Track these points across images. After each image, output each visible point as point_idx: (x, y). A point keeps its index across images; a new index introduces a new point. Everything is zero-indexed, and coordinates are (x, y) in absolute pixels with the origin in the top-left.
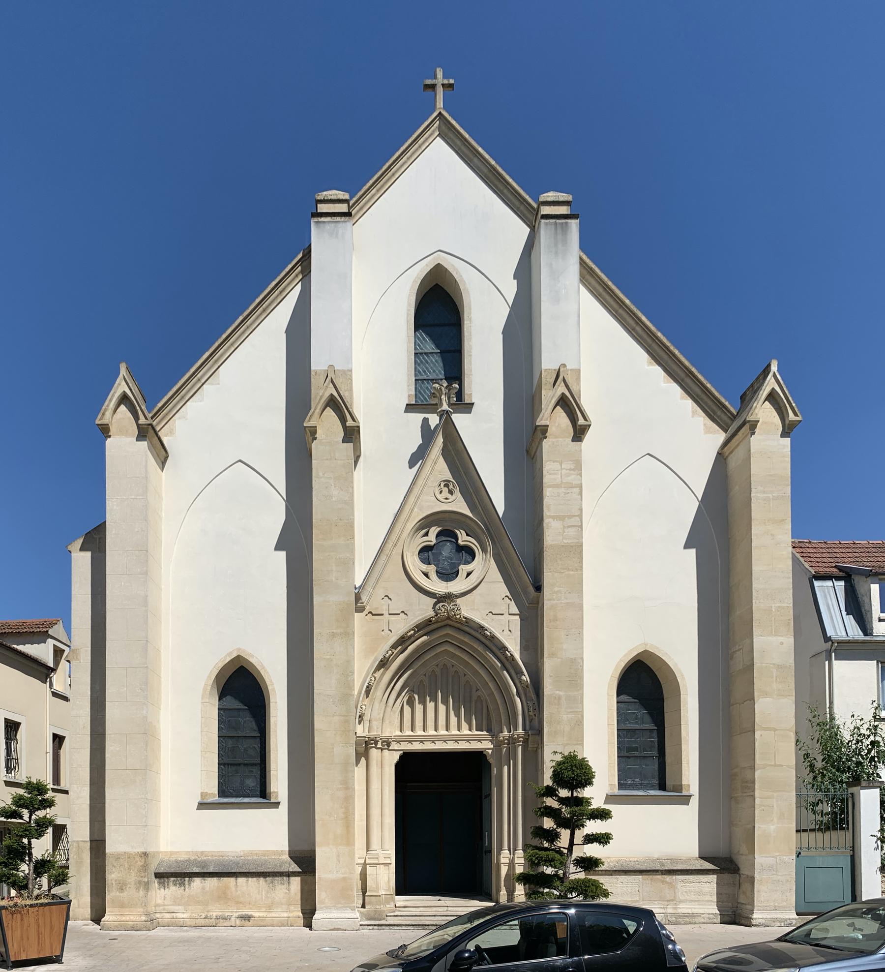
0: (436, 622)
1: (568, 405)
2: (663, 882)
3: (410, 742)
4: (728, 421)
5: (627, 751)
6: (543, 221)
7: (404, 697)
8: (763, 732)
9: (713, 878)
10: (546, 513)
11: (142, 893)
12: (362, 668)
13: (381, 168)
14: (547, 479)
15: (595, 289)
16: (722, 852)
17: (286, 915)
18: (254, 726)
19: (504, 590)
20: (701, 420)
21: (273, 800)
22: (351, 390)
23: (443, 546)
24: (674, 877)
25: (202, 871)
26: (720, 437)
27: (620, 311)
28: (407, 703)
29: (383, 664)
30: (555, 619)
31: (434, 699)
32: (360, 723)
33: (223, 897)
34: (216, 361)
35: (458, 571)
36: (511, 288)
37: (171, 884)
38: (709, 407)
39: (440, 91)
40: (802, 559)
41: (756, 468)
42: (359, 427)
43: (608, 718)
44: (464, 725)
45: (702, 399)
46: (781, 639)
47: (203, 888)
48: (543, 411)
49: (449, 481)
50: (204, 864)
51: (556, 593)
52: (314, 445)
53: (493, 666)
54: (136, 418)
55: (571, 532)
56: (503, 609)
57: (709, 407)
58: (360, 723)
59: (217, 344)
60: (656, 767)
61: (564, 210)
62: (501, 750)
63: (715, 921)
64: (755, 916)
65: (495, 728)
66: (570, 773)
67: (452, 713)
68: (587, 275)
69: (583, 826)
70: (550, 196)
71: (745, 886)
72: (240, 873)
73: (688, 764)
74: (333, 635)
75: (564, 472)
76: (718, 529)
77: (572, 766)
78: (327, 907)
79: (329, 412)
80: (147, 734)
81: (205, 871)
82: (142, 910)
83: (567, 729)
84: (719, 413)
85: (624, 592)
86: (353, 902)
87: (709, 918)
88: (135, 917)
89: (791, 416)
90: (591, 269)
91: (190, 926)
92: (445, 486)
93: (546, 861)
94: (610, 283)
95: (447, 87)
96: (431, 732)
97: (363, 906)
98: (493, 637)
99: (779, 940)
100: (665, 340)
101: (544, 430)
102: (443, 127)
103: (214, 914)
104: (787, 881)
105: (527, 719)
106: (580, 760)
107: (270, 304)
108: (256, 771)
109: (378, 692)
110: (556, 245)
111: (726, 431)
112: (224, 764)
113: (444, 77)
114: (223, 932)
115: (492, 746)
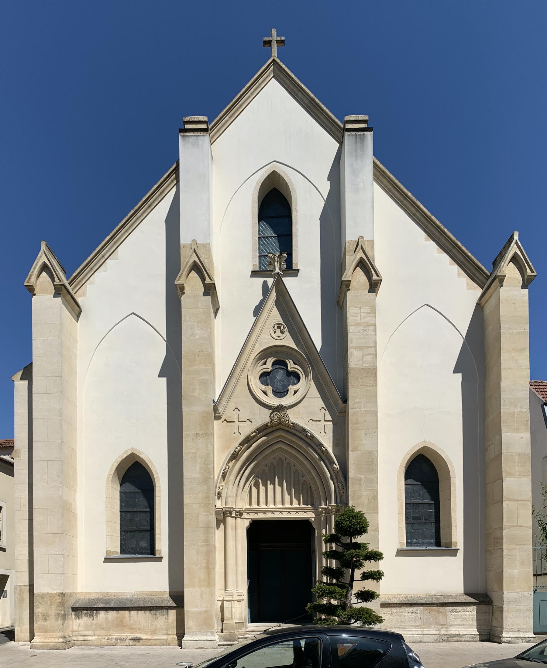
0: (272, 427)
1: (365, 265)
2: (438, 611)
3: (256, 513)
4: (484, 280)
5: (412, 520)
6: (346, 133)
7: (252, 481)
8: (508, 502)
9: (474, 608)
10: (350, 345)
11: (60, 622)
12: (220, 460)
13: (232, 100)
14: (350, 320)
15: (386, 186)
16: (480, 589)
17: (165, 637)
18: (146, 504)
19: (320, 403)
20: (465, 279)
21: (157, 556)
22: (210, 258)
23: (277, 372)
24: (446, 608)
25: (106, 606)
26: (479, 292)
27: (405, 202)
28: (255, 485)
29: (235, 457)
30: (357, 422)
31: (273, 482)
32: (219, 499)
33: (121, 625)
34: (115, 243)
35: (288, 390)
36: (325, 187)
37: (83, 615)
38: (470, 270)
39: (275, 46)
40: (536, 393)
41: (504, 311)
42: (214, 284)
43: (398, 495)
44: (295, 501)
45: (464, 265)
46: (521, 435)
47: (106, 618)
48: (347, 271)
49: (281, 324)
50: (108, 601)
51: (357, 403)
52: (182, 298)
53: (313, 458)
54: (53, 280)
55: (368, 358)
56: (320, 417)
57: (470, 270)
58: (219, 499)
59: (115, 230)
60: (433, 530)
61: (363, 126)
62: (321, 518)
63: (476, 639)
64: (504, 635)
65: (316, 502)
66: (348, 522)
67: (286, 492)
68: (379, 176)
69: (361, 565)
70: (353, 117)
71: (497, 614)
72: (132, 607)
73: (456, 527)
74: (197, 435)
75: (363, 314)
76: (477, 359)
77: (349, 517)
78: (194, 633)
79: (194, 274)
80: (66, 510)
81: (108, 606)
82: (60, 634)
83: (366, 502)
84: (477, 274)
85: (409, 403)
86: (213, 628)
87: (471, 637)
88: (55, 639)
89: (529, 272)
90: (383, 171)
91: (97, 646)
92: (278, 327)
93: (328, 593)
94: (397, 181)
95: (279, 42)
96: (271, 506)
97: (222, 631)
98: (312, 437)
99: (519, 657)
100: (437, 222)
101: (348, 284)
102: (276, 71)
103: (114, 637)
104: (527, 610)
105: (338, 495)
106: (357, 513)
107: (153, 202)
108: (147, 535)
109: (231, 477)
110: (356, 151)
111: (482, 288)
112: (124, 531)
113: (277, 36)
114: (119, 650)
115: (314, 516)
